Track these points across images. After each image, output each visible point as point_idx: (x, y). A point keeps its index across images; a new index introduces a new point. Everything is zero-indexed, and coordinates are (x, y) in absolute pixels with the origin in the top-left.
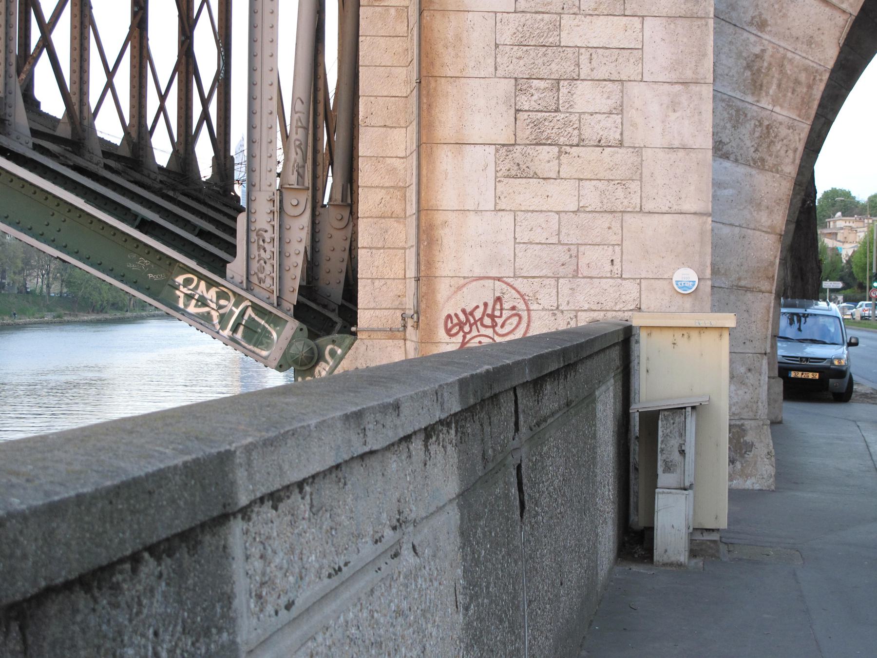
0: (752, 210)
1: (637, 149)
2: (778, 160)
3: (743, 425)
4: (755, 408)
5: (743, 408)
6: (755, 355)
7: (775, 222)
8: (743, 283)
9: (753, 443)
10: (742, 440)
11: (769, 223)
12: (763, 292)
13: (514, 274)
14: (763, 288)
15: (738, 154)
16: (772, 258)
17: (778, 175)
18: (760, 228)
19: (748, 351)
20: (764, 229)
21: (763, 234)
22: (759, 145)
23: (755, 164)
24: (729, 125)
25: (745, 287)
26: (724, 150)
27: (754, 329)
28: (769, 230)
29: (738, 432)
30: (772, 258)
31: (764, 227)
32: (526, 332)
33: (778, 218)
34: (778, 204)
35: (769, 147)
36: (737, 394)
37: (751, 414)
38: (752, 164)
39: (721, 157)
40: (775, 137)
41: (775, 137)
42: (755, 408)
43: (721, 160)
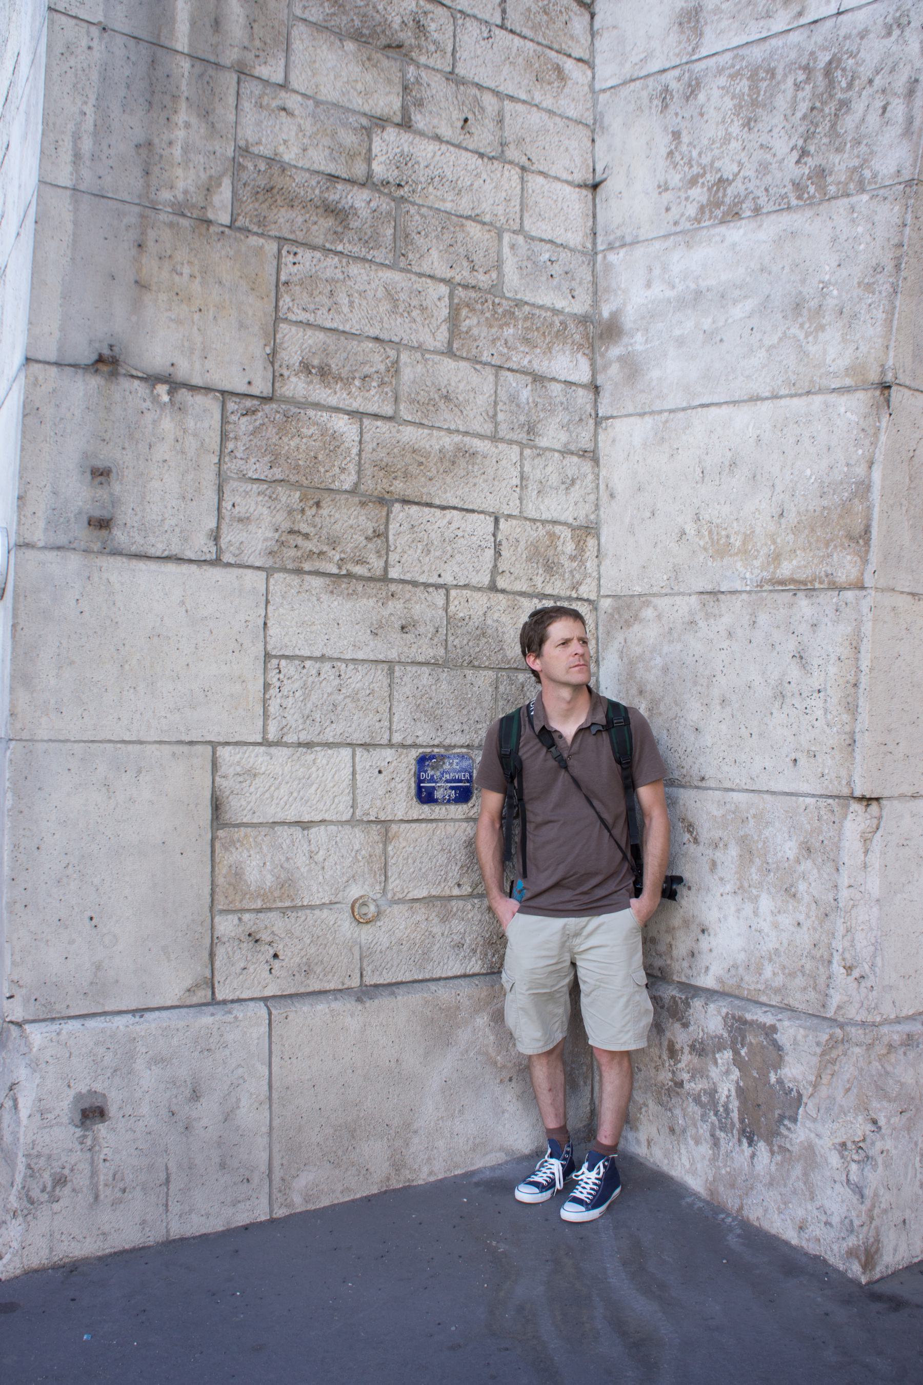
0: (801, 336)
1: (363, 40)
2: (863, 148)
3: (774, 1029)
4: (822, 980)
5: (792, 975)
6: (822, 803)
7: (864, 349)
8: (786, 569)
9: (800, 1096)
10: (773, 1078)
11: (845, 362)
12: (841, 589)
13: (391, 672)
14: (842, 577)
15: (760, 193)
16: (860, 471)
17: (865, 197)
18: (824, 382)
19: (805, 788)
20: (836, 384)
21: (832, 398)
22: (808, 136)
23: (799, 198)
24: (735, 129)
25: (793, 581)
26: (728, 200)
27: (819, 713)
28: (848, 382)
29: (763, 1047)
30: (860, 471)
31: (835, 375)
32: (589, 921)
33: (870, 332)
34: (869, 287)
35: (833, 126)
36: (776, 926)
37: (812, 995)
38: (794, 202)
39: (722, 222)
40: (850, 86)
41: (850, 86)
42: (822, 980)
43: (722, 229)
